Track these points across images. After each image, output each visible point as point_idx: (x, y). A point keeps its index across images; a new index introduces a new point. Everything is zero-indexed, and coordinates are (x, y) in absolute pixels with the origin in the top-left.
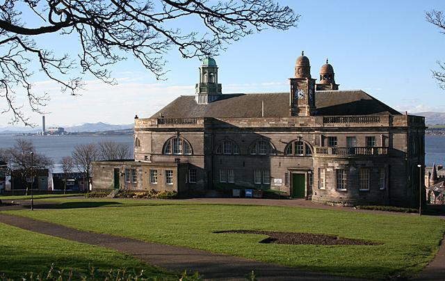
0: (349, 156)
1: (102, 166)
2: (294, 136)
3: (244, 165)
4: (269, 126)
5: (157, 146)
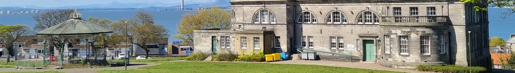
0: (432, 24)
1: (201, 34)
3: (321, 33)
5: (248, 17)
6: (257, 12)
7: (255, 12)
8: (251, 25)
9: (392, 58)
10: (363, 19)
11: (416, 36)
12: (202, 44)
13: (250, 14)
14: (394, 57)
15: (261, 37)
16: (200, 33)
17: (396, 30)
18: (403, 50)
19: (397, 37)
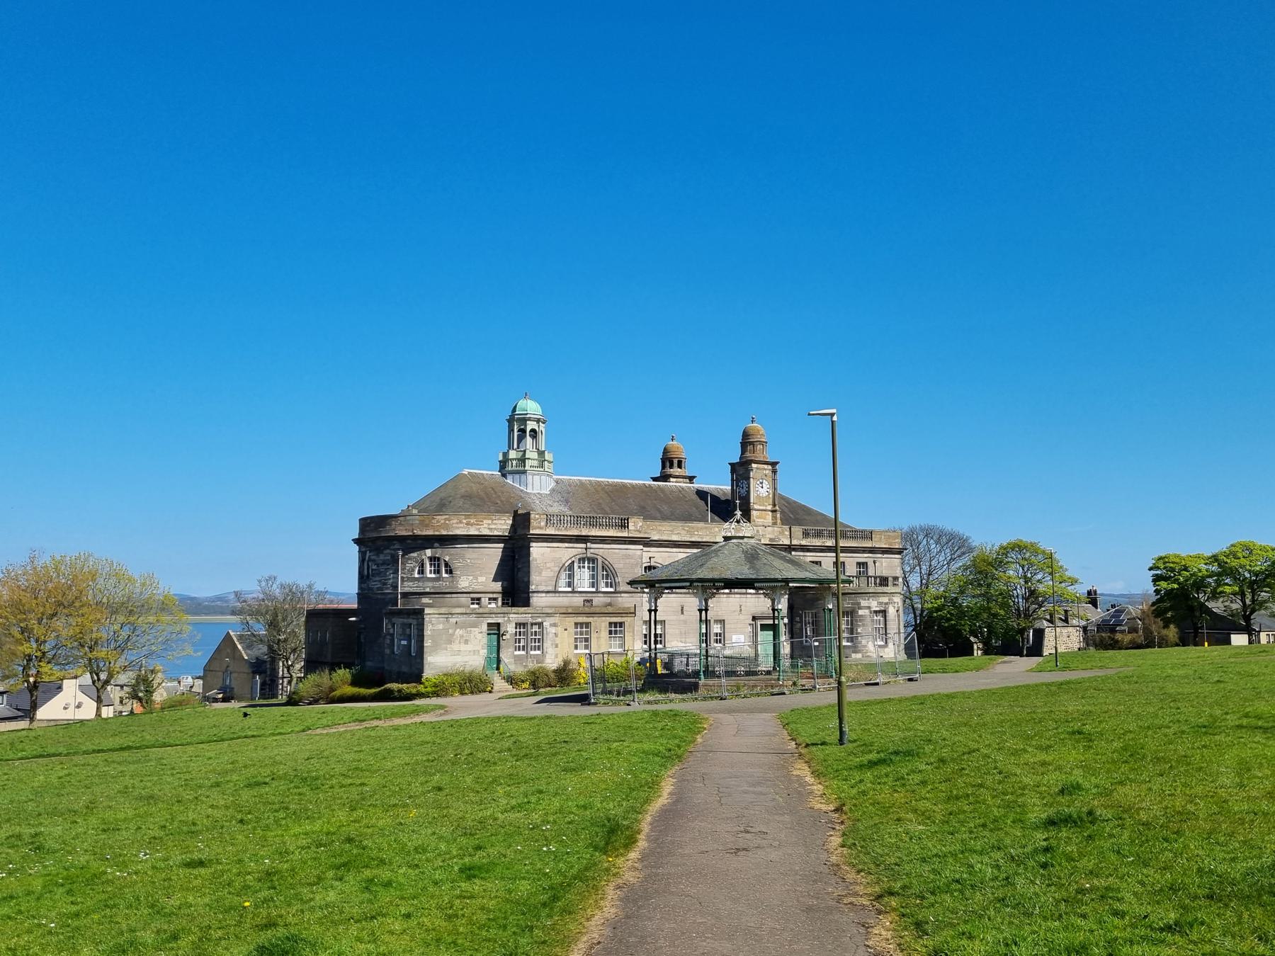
1: (453, 620)
3: (682, 613)
5: (544, 573)
6: (570, 561)
7: (563, 562)
8: (553, 595)
9: (860, 653)
12: (455, 647)
13: (549, 568)
14: (864, 651)
16: (450, 616)
17: (868, 600)
19: (871, 613)
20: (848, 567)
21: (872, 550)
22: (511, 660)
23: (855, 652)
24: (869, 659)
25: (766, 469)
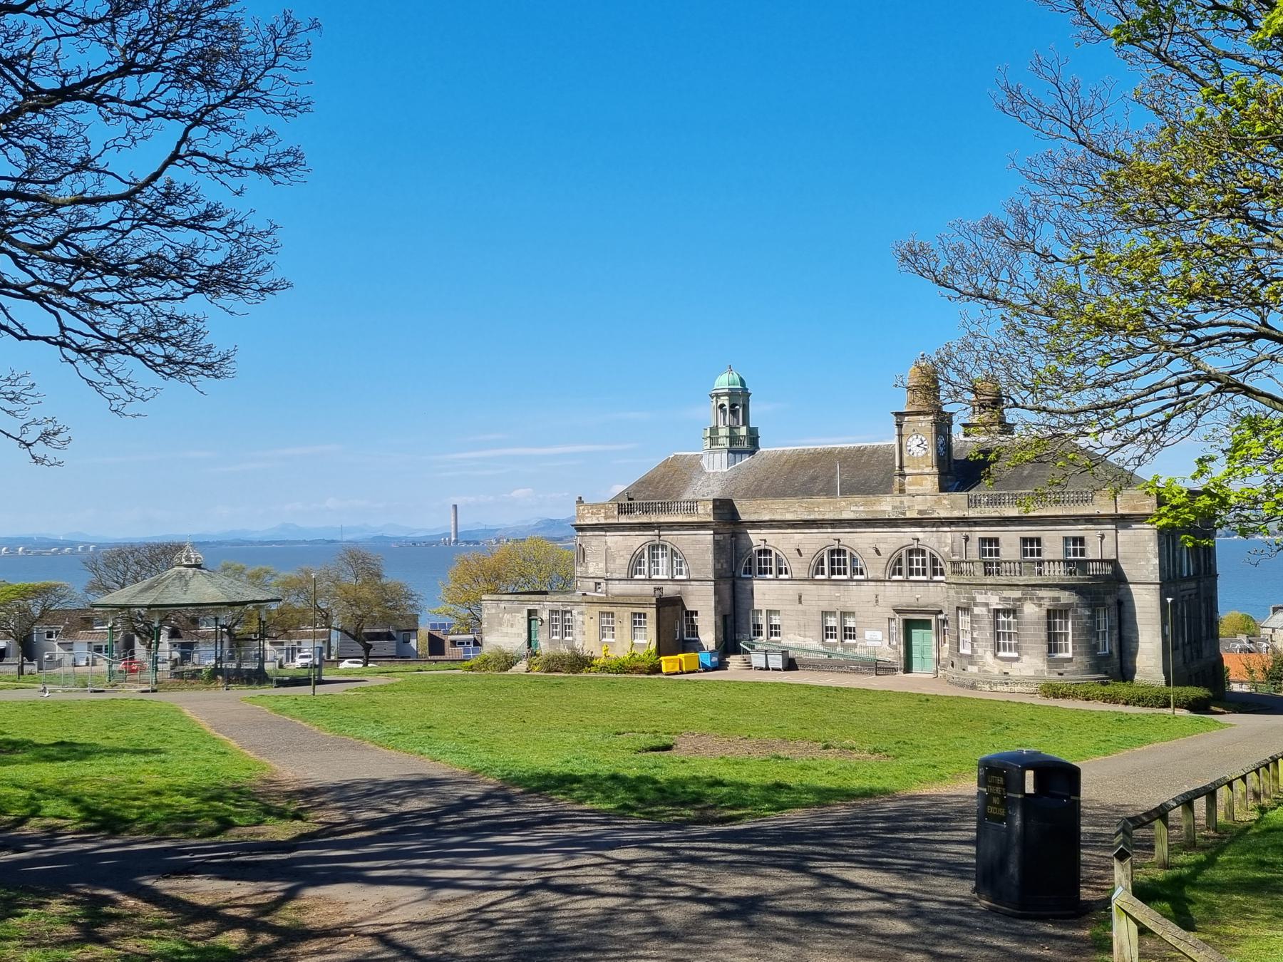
0: (1076, 579)
1: (502, 606)
2: (906, 536)
3: (800, 602)
4: (852, 516)
5: (618, 561)
10: (904, 566)
11: (1037, 609)
12: (504, 629)
15: (651, 612)
18: (1004, 644)
20: (1047, 544)
21: (1089, 519)
22: (545, 646)
23: (972, 664)
24: (986, 674)
25: (921, 422)
